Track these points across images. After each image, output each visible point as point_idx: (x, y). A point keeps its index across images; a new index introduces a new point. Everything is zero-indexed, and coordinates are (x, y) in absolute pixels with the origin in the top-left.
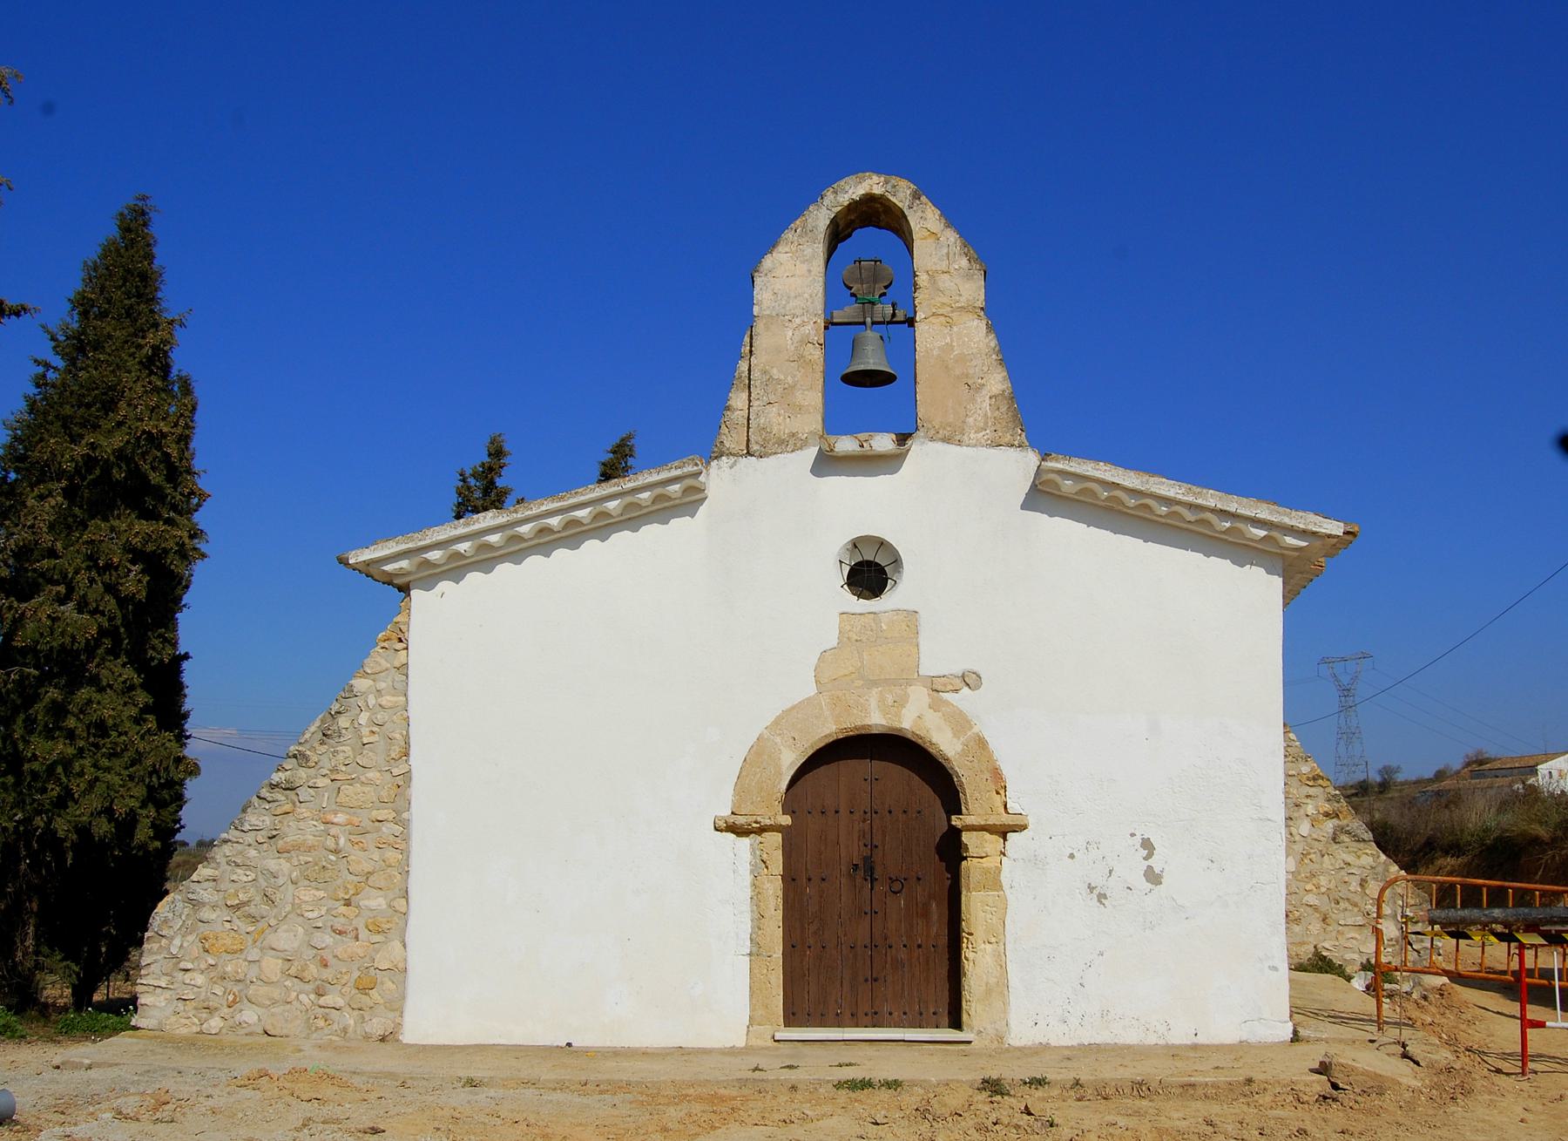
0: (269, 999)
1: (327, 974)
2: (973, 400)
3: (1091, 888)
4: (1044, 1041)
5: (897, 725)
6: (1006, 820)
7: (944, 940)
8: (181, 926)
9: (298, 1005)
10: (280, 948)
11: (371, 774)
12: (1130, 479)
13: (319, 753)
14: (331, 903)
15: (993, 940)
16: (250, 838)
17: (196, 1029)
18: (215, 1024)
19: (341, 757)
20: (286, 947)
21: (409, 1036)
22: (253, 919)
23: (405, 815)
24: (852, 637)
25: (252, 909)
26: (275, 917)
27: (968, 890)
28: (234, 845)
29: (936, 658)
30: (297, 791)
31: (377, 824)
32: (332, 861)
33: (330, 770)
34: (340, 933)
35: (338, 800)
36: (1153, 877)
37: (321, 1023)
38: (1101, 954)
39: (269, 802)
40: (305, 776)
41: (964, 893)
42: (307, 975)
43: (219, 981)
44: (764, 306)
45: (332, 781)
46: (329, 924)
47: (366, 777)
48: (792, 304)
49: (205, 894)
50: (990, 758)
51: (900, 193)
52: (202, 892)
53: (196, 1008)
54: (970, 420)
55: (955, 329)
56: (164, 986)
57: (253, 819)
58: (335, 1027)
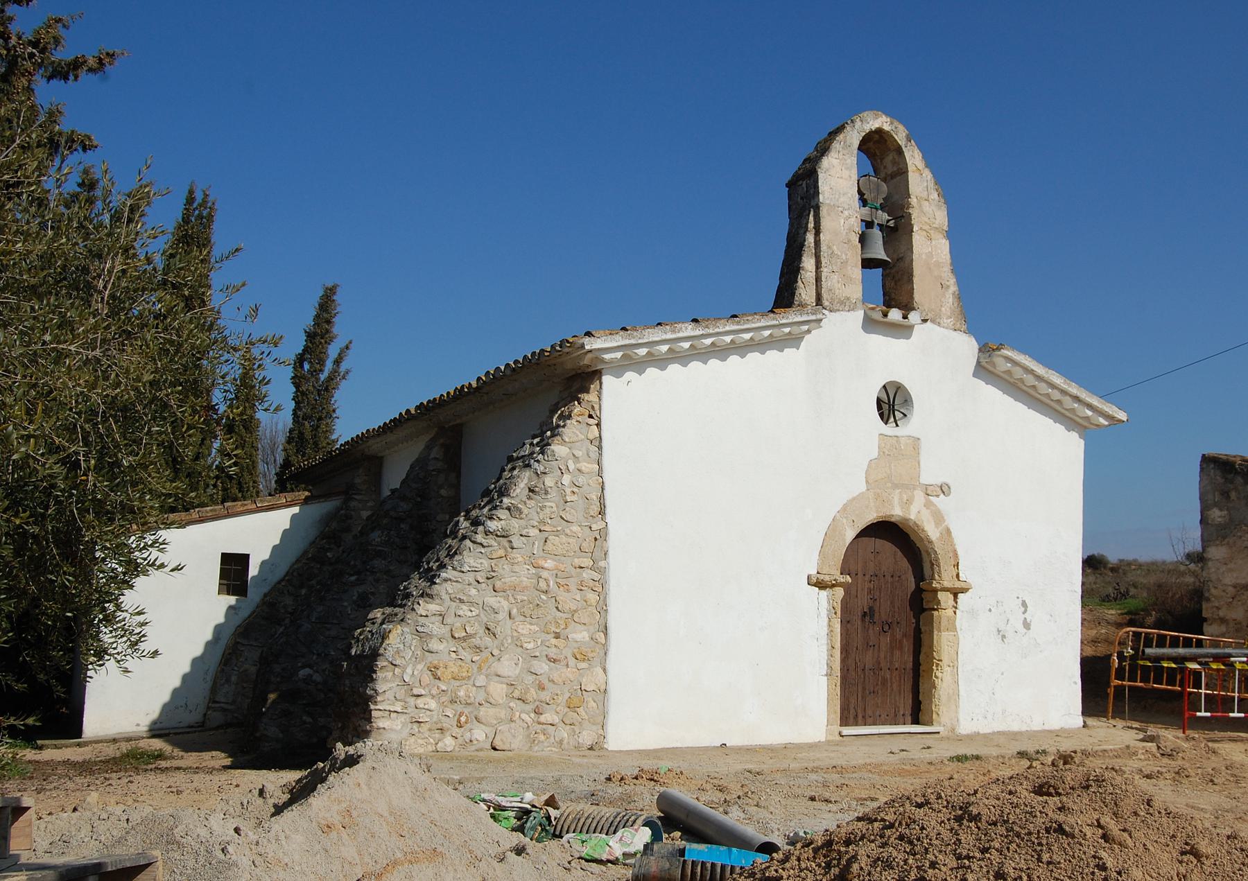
0: (496, 719)
1: (545, 696)
2: (944, 296)
3: (999, 631)
4: (976, 731)
5: (907, 516)
6: (958, 585)
7: (910, 665)
8: (412, 656)
9: (521, 723)
10: (506, 674)
11: (575, 528)
12: (1040, 370)
13: (530, 508)
14: (544, 636)
15: (951, 664)
16: (470, 577)
17: (430, 748)
18: (448, 743)
19: (547, 511)
20: (510, 674)
21: (613, 744)
22: (478, 649)
23: (602, 564)
24: (889, 452)
25: (476, 641)
26: (497, 647)
27: (939, 631)
28: (454, 583)
29: (930, 474)
30: (510, 538)
31: (578, 570)
32: (543, 600)
33: (539, 522)
34: (555, 661)
35: (546, 548)
36: (1027, 625)
37: (542, 737)
38: (1002, 674)
39: (483, 546)
40: (517, 526)
41: (935, 632)
42: (529, 697)
43: (449, 705)
44: (826, 196)
45: (540, 531)
46: (545, 653)
47: (571, 530)
48: (842, 200)
49: (434, 627)
50: (953, 545)
51: (900, 135)
52: (431, 625)
53: (430, 730)
54: (943, 309)
55: (934, 242)
56: (400, 711)
57: (472, 561)
58: (552, 740)
